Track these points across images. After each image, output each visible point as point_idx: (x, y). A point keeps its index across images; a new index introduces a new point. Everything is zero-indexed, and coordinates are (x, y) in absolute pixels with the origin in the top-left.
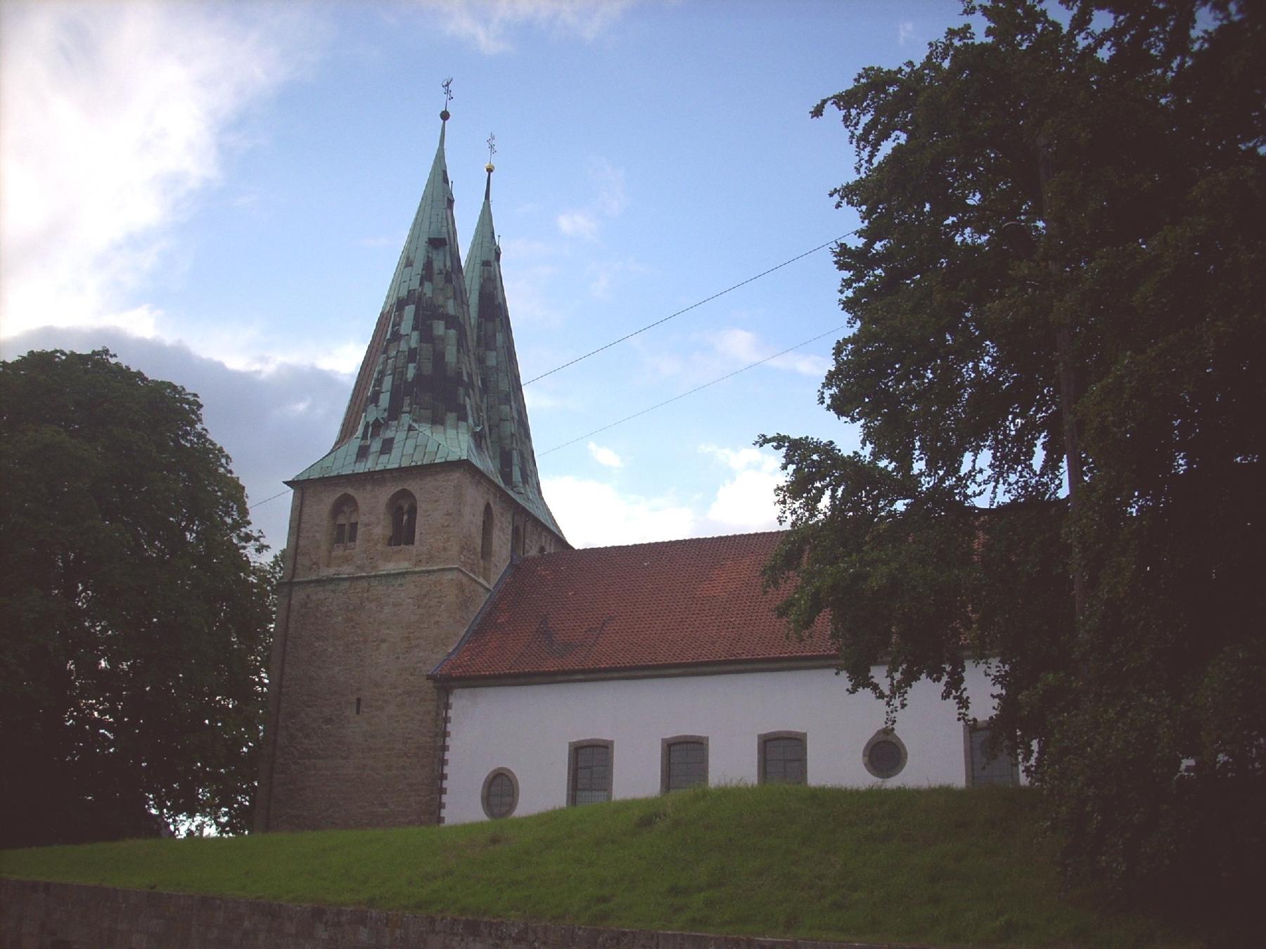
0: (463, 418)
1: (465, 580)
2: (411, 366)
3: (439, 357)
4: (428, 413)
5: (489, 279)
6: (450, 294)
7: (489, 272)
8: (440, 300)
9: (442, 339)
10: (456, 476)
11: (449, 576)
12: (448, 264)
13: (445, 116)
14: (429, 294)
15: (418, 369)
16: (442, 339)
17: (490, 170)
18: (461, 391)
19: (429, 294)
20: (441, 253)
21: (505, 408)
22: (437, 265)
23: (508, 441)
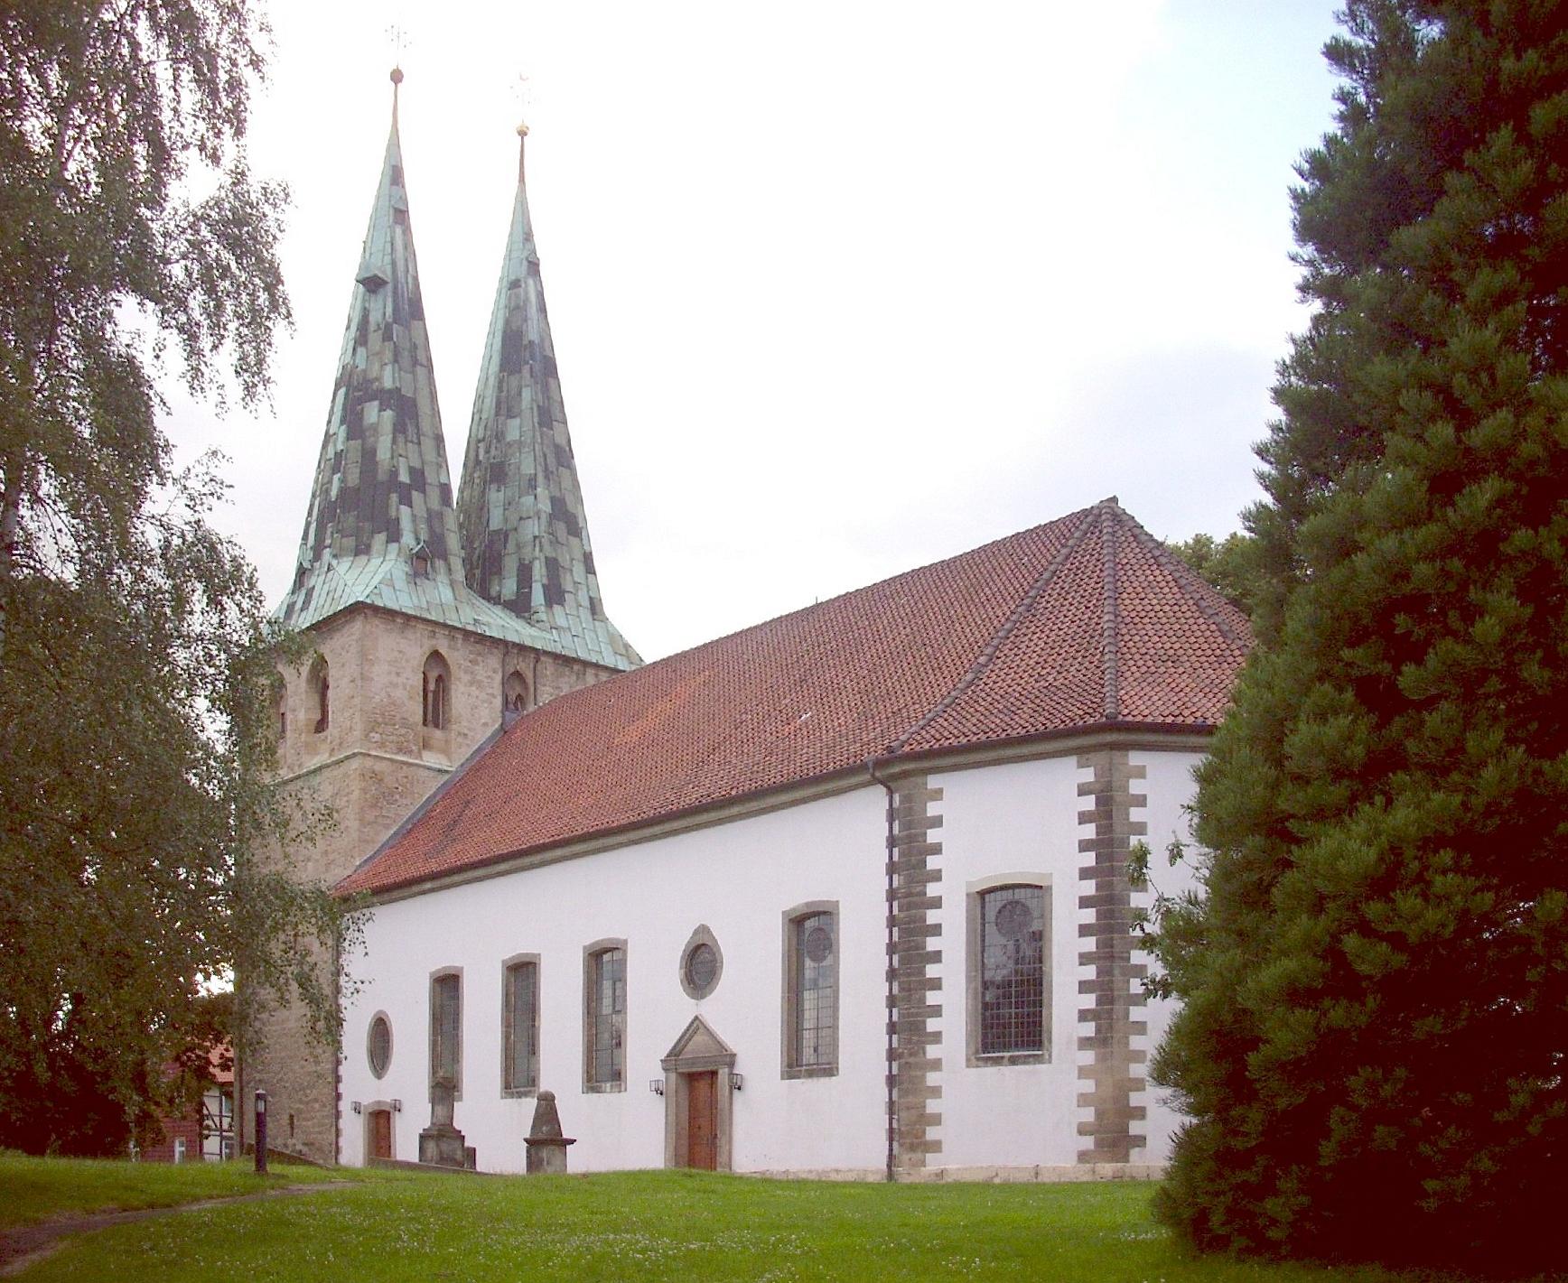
0: (394, 536)
1: (369, 763)
2: (336, 477)
3: (369, 455)
4: (350, 542)
5: (517, 307)
6: (388, 356)
7: (517, 296)
8: (374, 373)
9: (375, 428)
10: (358, 626)
11: (355, 764)
12: (389, 310)
13: (397, 77)
14: (362, 366)
15: (342, 481)
16: (375, 428)
17: (522, 134)
18: (394, 497)
19: (362, 366)
20: (380, 297)
21: (528, 500)
22: (375, 317)
23: (530, 548)
